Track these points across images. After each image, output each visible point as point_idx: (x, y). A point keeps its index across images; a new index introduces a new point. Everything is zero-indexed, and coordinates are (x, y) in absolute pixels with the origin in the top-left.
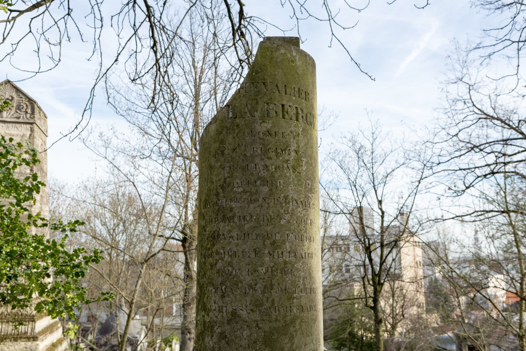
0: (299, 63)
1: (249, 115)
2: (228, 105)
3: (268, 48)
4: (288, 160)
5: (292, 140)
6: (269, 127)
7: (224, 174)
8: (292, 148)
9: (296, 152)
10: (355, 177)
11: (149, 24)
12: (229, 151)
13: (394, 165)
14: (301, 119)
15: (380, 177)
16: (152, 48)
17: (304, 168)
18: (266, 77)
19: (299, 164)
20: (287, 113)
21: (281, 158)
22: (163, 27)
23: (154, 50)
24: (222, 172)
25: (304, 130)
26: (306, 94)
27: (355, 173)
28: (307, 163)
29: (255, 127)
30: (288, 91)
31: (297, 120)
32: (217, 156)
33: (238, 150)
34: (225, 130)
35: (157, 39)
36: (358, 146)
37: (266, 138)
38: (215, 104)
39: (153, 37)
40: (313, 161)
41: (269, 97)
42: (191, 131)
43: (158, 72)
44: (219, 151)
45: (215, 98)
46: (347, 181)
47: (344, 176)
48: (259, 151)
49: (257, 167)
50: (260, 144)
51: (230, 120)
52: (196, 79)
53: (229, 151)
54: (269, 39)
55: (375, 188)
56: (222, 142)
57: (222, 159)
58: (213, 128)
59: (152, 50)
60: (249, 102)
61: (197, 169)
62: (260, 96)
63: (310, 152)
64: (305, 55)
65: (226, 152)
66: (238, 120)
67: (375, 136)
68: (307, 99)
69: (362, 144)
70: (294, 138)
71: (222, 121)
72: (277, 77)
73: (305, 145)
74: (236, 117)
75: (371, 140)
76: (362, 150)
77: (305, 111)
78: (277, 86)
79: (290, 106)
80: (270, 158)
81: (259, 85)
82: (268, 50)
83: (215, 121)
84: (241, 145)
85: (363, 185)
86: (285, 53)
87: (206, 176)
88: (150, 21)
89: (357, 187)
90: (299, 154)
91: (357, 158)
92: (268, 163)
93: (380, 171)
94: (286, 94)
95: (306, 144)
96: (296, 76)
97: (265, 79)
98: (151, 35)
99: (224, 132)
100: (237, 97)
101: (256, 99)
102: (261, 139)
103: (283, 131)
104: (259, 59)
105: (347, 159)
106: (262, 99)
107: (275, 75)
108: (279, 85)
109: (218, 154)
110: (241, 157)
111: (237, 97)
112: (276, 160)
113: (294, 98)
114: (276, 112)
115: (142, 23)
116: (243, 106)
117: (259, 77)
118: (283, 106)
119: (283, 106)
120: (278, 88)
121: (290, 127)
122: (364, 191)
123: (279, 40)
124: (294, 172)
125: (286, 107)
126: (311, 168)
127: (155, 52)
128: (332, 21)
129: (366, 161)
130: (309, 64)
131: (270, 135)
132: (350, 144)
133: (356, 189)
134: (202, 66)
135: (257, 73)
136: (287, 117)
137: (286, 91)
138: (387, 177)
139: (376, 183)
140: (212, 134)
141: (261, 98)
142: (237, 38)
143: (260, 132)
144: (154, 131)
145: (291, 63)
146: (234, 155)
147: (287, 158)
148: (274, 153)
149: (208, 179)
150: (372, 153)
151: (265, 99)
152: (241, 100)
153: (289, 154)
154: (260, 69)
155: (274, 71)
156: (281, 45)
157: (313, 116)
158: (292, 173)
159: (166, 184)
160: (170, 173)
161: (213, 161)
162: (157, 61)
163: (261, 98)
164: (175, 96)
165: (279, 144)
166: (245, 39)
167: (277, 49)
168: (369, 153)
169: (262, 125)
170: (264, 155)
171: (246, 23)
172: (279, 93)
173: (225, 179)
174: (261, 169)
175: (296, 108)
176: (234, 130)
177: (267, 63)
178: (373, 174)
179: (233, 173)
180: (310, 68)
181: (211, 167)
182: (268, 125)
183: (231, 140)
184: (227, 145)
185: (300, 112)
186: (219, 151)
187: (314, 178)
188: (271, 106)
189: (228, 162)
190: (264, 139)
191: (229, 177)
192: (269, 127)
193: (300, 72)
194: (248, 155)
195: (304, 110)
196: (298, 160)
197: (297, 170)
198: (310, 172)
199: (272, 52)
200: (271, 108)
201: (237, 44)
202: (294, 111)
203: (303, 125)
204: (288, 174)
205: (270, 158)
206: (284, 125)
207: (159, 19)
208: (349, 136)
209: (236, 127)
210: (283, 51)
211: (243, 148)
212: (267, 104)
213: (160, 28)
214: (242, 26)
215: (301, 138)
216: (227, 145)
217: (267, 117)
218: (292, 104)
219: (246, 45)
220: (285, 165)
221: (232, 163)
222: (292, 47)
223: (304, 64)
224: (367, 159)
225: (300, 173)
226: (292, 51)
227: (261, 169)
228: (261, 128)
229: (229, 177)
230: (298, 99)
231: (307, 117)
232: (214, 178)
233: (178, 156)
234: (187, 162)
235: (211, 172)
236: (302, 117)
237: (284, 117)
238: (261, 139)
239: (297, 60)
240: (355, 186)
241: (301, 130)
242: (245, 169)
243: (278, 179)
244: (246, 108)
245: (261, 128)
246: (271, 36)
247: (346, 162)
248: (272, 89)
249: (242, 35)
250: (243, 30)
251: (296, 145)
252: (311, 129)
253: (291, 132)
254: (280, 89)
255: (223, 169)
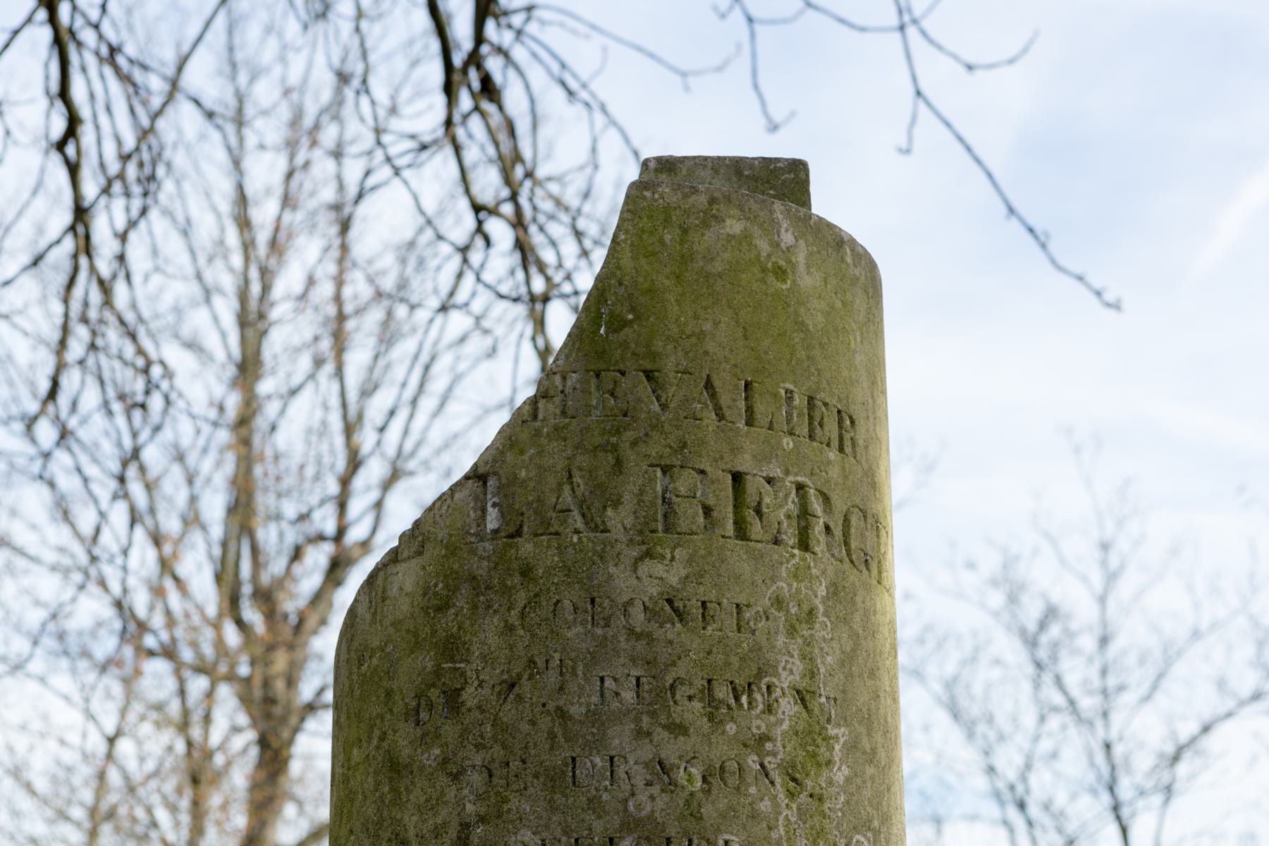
0: (808, 280)
1: (580, 524)
2: (477, 476)
3: (667, 210)
4: (764, 738)
5: (781, 640)
6: (674, 580)
7: (460, 803)
8: (784, 680)
9: (802, 697)
10: (1019, 760)
11: (46, 33)
12: (486, 691)
13: (1207, 702)
14: (822, 538)
15: (1143, 762)
16: (60, 146)
17: (840, 774)
18: (658, 344)
19: (814, 755)
20: (758, 512)
21: (731, 728)
22: (114, 50)
23: (67, 161)
24: (451, 793)
25: (835, 591)
26: (842, 423)
27: (1022, 740)
28: (852, 747)
29: (610, 576)
30: (760, 408)
31: (804, 545)
32: (424, 716)
33: (525, 688)
34: (465, 590)
35: (85, 112)
36: (1031, 613)
37: (658, 633)
38: (335, 401)
39: (64, 93)
40: (878, 737)
41: (672, 440)
42: (217, 532)
43: (83, 261)
44: (434, 693)
45: (339, 373)
46: (981, 782)
47: (966, 755)
48: (628, 696)
49: (621, 771)
50: (633, 660)
51: (488, 546)
52: (246, 281)
53: (486, 691)
54: (664, 167)
55: (1118, 818)
56: (451, 648)
57: (450, 731)
58: (407, 578)
59: (56, 157)
60: (582, 460)
61: (243, 719)
62: (629, 435)
63: (863, 698)
64: (834, 243)
65: (470, 696)
66: (526, 547)
67: (1114, 562)
68: (847, 443)
69: (1056, 598)
70: (792, 631)
71: (452, 550)
72: (710, 346)
73: (842, 663)
74: (518, 533)
75: (1097, 579)
76: (1055, 631)
77: (839, 504)
78: (709, 385)
79: (769, 481)
80: (679, 729)
81: (625, 383)
82: (667, 220)
83: (415, 547)
84: (541, 663)
85: (1061, 799)
86: (746, 237)
87: (371, 811)
88: (53, 20)
89: (1034, 811)
90: (813, 705)
91: (1030, 669)
92: (672, 749)
93: (1143, 731)
94: (749, 423)
95: (848, 659)
96: (797, 337)
97: (654, 356)
98: (55, 86)
99: (461, 602)
100: (524, 436)
101: (615, 448)
102: (639, 636)
103: (741, 599)
104: (626, 261)
105: (984, 674)
106: (642, 448)
107: (701, 336)
108: (717, 384)
109: (431, 707)
110: (545, 723)
111: (524, 436)
112: (707, 737)
113: (788, 443)
114: (707, 510)
115: (16, 33)
116: (552, 481)
117: (625, 345)
118: (738, 478)
119: (738, 478)
120: (713, 396)
121: (773, 579)
122: (1071, 828)
123: (716, 171)
124: (791, 795)
125: (754, 485)
126: (870, 771)
127: (73, 170)
128: (912, 31)
129: (1072, 680)
130: (855, 280)
131: (680, 615)
132: (997, 599)
133: (1030, 824)
134: (279, 219)
135: (617, 324)
136: (756, 529)
137: (750, 410)
138: (1176, 758)
139: (1125, 789)
140: (404, 607)
141: (634, 444)
142: (465, 101)
143: (630, 602)
144: (34, 527)
145: (771, 278)
146: (508, 713)
147: (759, 725)
148: (697, 705)
149: (379, 824)
150: (1104, 641)
151: (655, 449)
152: (540, 453)
153: (769, 709)
154: (633, 310)
155: (696, 317)
156: (728, 199)
157: (875, 524)
158: (782, 798)
159: (88, 796)
160: (111, 741)
161: (403, 739)
162: (81, 213)
163: (634, 444)
164: (156, 371)
165: (719, 658)
166: (501, 108)
167: (710, 217)
168: (1088, 643)
169: (644, 568)
170: (653, 714)
171: (507, 38)
172: (721, 417)
173: (465, 826)
174: (639, 782)
175: (800, 487)
176: (507, 590)
177: (664, 281)
178: (1108, 746)
179: (505, 801)
180: (860, 303)
181: (395, 768)
182: (668, 572)
183: (493, 640)
184: (477, 663)
185: (816, 506)
186: (434, 693)
187: (886, 819)
188: (684, 482)
189: (479, 747)
190: (649, 638)
191: (482, 819)
192: (674, 580)
193: (816, 320)
194: (576, 710)
195: (834, 498)
196: (812, 736)
197: (809, 783)
198: (867, 793)
199: (685, 231)
200: (683, 491)
201: (460, 133)
202: (792, 506)
203: (830, 571)
204: (765, 806)
205: (679, 729)
206: (746, 568)
207: (94, 15)
208: (990, 563)
209: (517, 579)
210: (734, 226)
211: (552, 678)
212: (666, 470)
213: (97, 54)
214: (485, 49)
215: (822, 629)
216: (477, 663)
217: (666, 531)
218: (778, 472)
219: (503, 137)
220: (752, 762)
221: (498, 752)
222: (778, 206)
223: (833, 282)
224: (1076, 672)
225: (820, 799)
226: (775, 224)
227: (639, 782)
228: (639, 583)
229: (482, 819)
230: (810, 448)
231: (848, 533)
232: (411, 821)
233: (151, 653)
234: (198, 684)
235: (395, 790)
236: (827, 528)
237: (742, 532)
238: (639, 636)
239: (802, 268)
240: (1022, 806)
241: (822, 591)
242: (562, 779)
243: (718, 831)
244: (567, 488)
245: (639, 583)
246: (679, 152)
247: (978, 689)
248: (686, 401)
249: (489, 89)
250: (494, 65)
251: (798, 666)
252: (868, 588)
253: (778, 602)
254: (724, 400)
255: (455, 777)
